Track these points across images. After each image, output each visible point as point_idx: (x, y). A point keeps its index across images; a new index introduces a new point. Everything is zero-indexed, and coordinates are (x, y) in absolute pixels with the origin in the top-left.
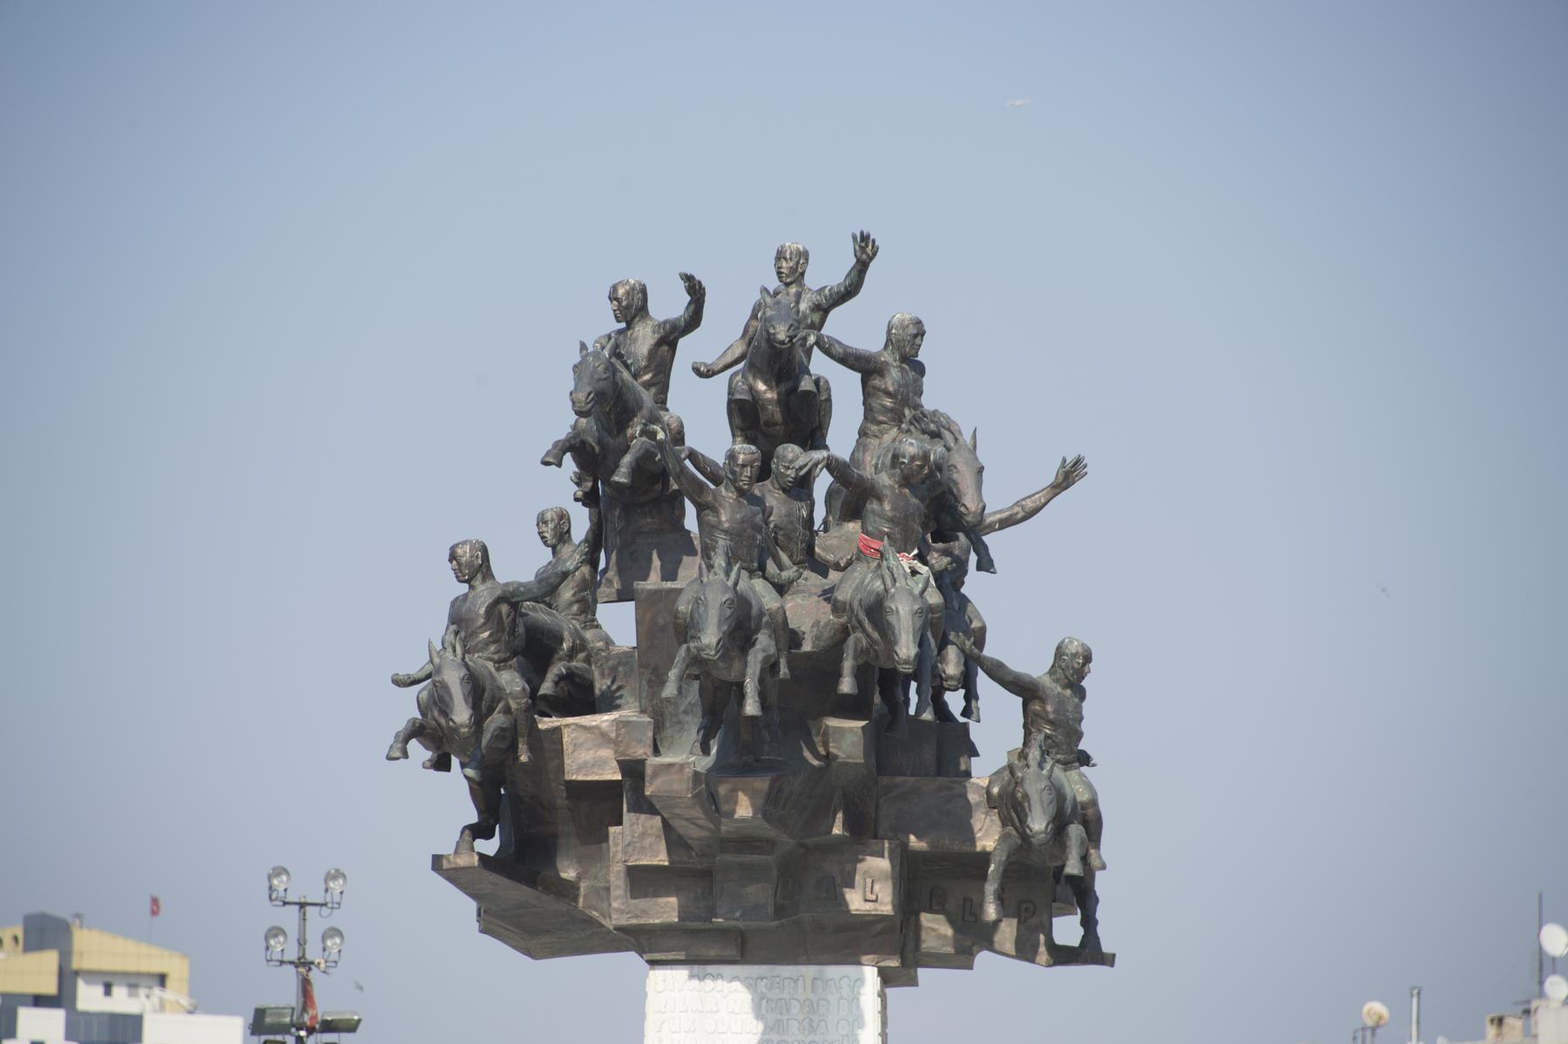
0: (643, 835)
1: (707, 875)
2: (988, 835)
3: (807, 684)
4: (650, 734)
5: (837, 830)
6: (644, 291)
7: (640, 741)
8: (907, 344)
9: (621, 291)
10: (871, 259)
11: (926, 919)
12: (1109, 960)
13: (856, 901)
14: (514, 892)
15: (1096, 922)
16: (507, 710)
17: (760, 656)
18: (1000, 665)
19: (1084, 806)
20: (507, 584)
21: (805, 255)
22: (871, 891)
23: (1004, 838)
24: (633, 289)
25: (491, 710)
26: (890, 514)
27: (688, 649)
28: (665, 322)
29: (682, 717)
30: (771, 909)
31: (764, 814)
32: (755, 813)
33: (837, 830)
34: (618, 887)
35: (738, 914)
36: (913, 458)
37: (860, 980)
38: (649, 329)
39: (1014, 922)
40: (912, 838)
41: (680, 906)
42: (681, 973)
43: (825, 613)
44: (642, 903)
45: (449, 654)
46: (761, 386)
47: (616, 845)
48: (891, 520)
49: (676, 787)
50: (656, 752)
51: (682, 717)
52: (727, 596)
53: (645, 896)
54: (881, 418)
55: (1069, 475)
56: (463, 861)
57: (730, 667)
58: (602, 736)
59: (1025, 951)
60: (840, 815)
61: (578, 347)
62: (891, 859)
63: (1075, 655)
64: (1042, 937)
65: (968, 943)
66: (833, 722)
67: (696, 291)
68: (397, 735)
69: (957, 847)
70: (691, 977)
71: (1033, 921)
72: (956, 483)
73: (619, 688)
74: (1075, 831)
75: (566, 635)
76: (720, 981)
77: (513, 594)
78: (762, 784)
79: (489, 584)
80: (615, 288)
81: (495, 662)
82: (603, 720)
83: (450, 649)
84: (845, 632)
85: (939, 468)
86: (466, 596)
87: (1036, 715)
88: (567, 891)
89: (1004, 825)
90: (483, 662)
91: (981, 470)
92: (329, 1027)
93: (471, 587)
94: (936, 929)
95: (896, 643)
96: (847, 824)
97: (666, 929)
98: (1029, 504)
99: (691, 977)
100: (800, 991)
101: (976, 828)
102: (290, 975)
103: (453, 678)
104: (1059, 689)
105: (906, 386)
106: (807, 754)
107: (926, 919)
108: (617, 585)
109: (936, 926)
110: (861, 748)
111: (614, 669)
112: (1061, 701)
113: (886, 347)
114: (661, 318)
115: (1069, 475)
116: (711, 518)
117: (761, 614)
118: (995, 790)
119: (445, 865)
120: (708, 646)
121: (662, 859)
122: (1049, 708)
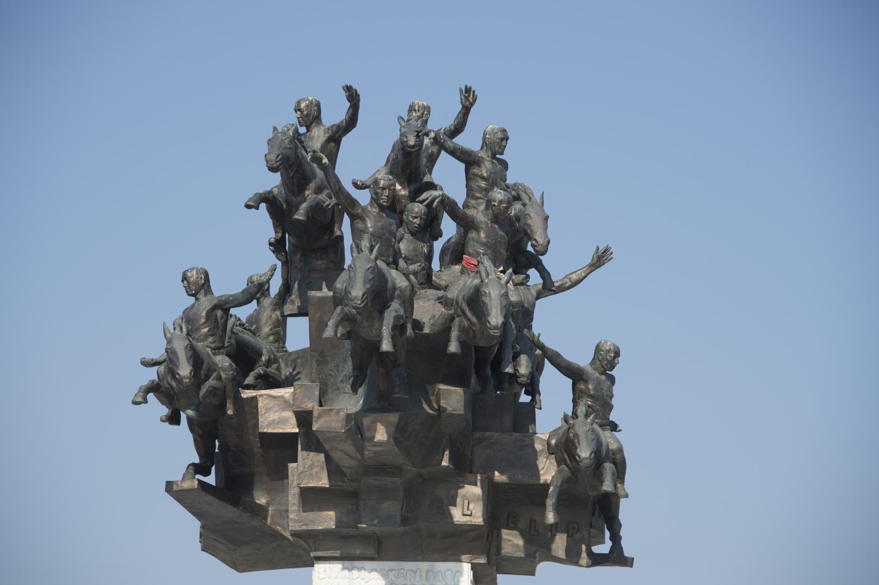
0: (311, 467)
1: (354, 495)
2: (548, 471)
4: (317, 393)
5: (445, 463)
6: (318, 105)
7: (310, 398)
8: (497, 144)
9: (303, 105)
10: (472, 105)
11: (506, 534)
12: (627, 562)
13: (457, 515)
14: (227, 511)
15: (620, 538)
16: (219, 378)
17: (393, 314)
18: (558, 355)
19: (614, 453)
20: (221, 297)
21: (427, 109)
22: (468, 507)
23: (559, 472)
24: (311, 103)
25: (207, 377)
26: (484, 240)
27: (342, 309)
28: (332, 126)
29: (339, 385)
30: (398, 519)
31: (395, 439)
32: (389, 438)
33: (445, 463)
34: (294, 504)
35: (376, 522)
36: (501, 202)
37: (460, 573)
38: (322, 131)
39: (565, 536)
40: (497, 473)
41: (336, 517)
42: (336, 567)
43: (440, 310)
44: (310, 515)
45: (178, 332)
46: (398, 187)
47: (293, 476)
48: (485, 245)
49: (334, 425)
50: (321, 405)
51: (339, 385)
52: (370, 265)
53: (312, 511)
54: (478, 195)
55: (601, 259)
56: (186, 485)
57: (372, 325)
59: (572, 558)
60: (447, 453)
61: (272, 130)
62: (482, 488)
63: (609, 351)
64: (584, 547)
65: (533, 550)
66: (442, 387)
67: (353, 97)
68: (141, 388)
69: (526, 480)
70: (344, 568)
71: (578, 536)
72: (529, 226)
73: (298, 373)
74: (608, 467)
75: (264, 351)
76: (363, 572)
77: (225, 302)
78: (394, 418)
79: (209, 297)
80: (299, 103)
81: (213, 349)
82: (286, 392)
83: (178, 328)
84: (452, 319)
85: (518, 219)
86: (193, 305)
87: (582, 391)
88: (260, 512)
89: (559, 465)
90: (204, 347)
91: (546, 218)
93: (197, 299)
94: (512, 542)
95: (488, 315)
96: (452, 459)
97: (327, 534)
98: (574, 277)
99: (344, 568)
100: (418, 579)
101: (540, 467)
103: (180, 346)
104: (597, 375)
105: (495, 173)
106: (425, 406)
107: (506, 534)
108: (298, 303)
109: (511, 538)
110: (462, 403)
111: (295, 361)
112: (598, 383)
113: (482, 148)
114: (329, 125)
115: (601, 259)
116: (360, 225)
117: (394, 288)
118: (553, 442)
119: (175, 488)
120: (356, 298)
122: (590, 387)
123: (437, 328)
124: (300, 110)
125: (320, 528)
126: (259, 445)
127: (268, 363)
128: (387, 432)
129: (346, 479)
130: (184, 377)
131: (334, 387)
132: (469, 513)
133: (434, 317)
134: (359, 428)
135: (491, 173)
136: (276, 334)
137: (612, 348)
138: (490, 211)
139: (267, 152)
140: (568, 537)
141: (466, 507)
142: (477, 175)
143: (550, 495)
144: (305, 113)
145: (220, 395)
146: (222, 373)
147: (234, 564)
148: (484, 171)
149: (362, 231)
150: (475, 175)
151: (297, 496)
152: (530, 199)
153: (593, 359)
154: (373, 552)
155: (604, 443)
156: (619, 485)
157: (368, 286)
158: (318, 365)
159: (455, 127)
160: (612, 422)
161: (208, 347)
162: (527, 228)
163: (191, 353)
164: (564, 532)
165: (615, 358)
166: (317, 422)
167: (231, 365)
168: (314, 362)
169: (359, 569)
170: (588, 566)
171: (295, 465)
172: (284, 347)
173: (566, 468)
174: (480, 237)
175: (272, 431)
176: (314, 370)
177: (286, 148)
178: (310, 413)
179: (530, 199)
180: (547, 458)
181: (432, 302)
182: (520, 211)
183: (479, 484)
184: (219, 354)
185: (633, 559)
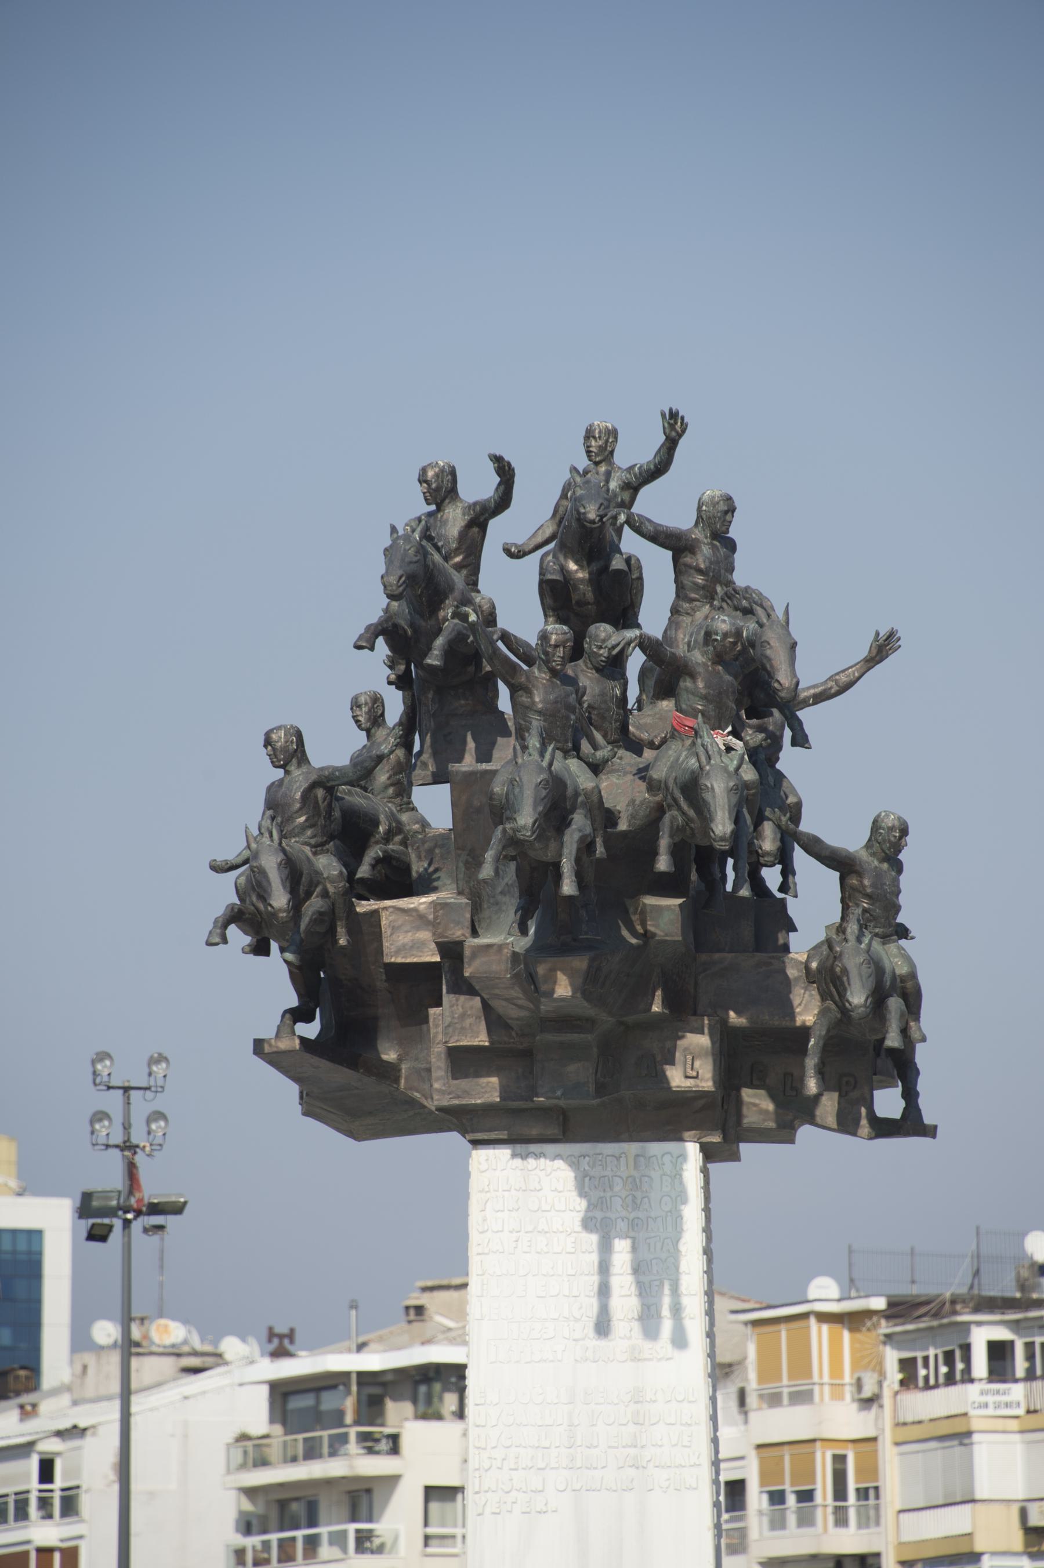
0: (463, 1016)
1: (527, 1054)
2: (807, 1010)
3: (624, 863)
4: (468, 916)
6: (453, 472)
7: (458, 923)
8: (718, 520)
9: (430, 474)
10: (680, 436)
11: (748, 1095)
13: (676, 1078)
15: (917, 1094)
16: (325, 894)
17: (576, 836)
18: (817, 840)
19: (903, 979)
21: (613, 433)
22: (692, 1067)
24: (442, 470)
25: (309, 895)
26: (703, 691)
27: (504, 831)
28: (475, 504)
29: (499, 897)
30: (592, 1088)
32: (574, 992)
33: (656, 1008)
34: (439, 1068)
35: (559, 1093)
36: (725, 635)
37: (683, 1156)
38: (459, 511)
39: (836, 1095)
40: (732, 1014)
42: (503, 1153)
43: (640, 792)
44: (464, 1084)
45: (266, 840)
46: (572, 566)
48: (704, 698)
49: (495, 967)
50: (475, 933)
51: (499, 897)
52: (542, 777)
53: (466, 1076)
54: (693, 595)
55: (883, 648)
56: (284, 1045)
58: (419, 919)
59: (847, 1124)
60: (659, 993)
63: (892, 829)
64: (863, 1110)
69: (776, 1022)
70: (514, 1155)
71: (855, 1094)
72: (769, 659)
73: (436, 870)
74: (895, 1003)
75: (382, 818)
76: (542, 1160)
77: (329, 778)
78: (580, 963)
79: (304, 769)
80: (424, 470)
81: (312, 846)
82: (421, 902)
83: (267, 835)
85: (752, 644)
86: (281, 781)
87: (854, 889)
88: (389, 1073)
90: (300, 847)
91: (794, 645)
92: (155, 1209)
93: (287, 772)
94: (757, 1104)
96: (665, 1002)
97: (488, 1109)
98: (843, 679)
99: (514, 1155)
101: (796, 1002)
102: (116, 1160)
103: (271, 863)
104: (876, 863)
105: (718, 562)
106: (625, 933)
107: (748, 1095)
108: (432, 768)
109: (757, 1101)
111: (430, 852)
112: (878, 875)
115: (883, 648)
116: (524, 699)
117: (577, 794)
118: (814, 965)
119: (267, 1049)
120: (524, 827)
121: (482, 1039)
122: (866, 882)
123: (638, 822)
124: (426, 482)
125: (479, 1101)
126: (384, 977)
127: (388, 837)
128: (571, 985)
129: (514, 1034)
130: (280, 910)
131: (492, 900)
132: (694, 1074)
133: (633, 801)
134: (531, 975)
135: (711, 563)
136: (397, 784)
137: (897, 823)
138: (711, 648)
139: (383, 571)
140: (840, 1096)
141: (689, 1066)
142: (690, 567)
143: (810, 1052)
144: (434, 486)
145: (327, 921)
146: (329, 886)
147: (351, 1132)
148: (701, 560)
149: (527, 708)
150: (686, 565)
151: (443, 1056)
152: (769, 616)
153: (870, 840)
154: (556, 1131)
155: (888, 969)
156: (912, 1024)
157: (541, 808)
158: (467, 869)
159: (655, 466)
160: (901, 925)
161: (306, 844)
162: (765, 661)
163: (286, 872)
164: (834, 1090)
165: (901, 838)
166: (470, 965)
167: (341, 873)
168: (461, 865)
169: (537, 1156)
170: (871, 1139)
171: (438, 1010)
172: (410, 803)
173: (833, 1006)
174: (697, 687)
175: (403, 961)
176: (461, 876)
177: (411, 562)
178: (460, 944)
179: (769, 616)
180: (806, 989)
181: (630, 777)
182: (755, 634)
183: (706, 1030)
184: (322, 852)
185: (936, 1127)
